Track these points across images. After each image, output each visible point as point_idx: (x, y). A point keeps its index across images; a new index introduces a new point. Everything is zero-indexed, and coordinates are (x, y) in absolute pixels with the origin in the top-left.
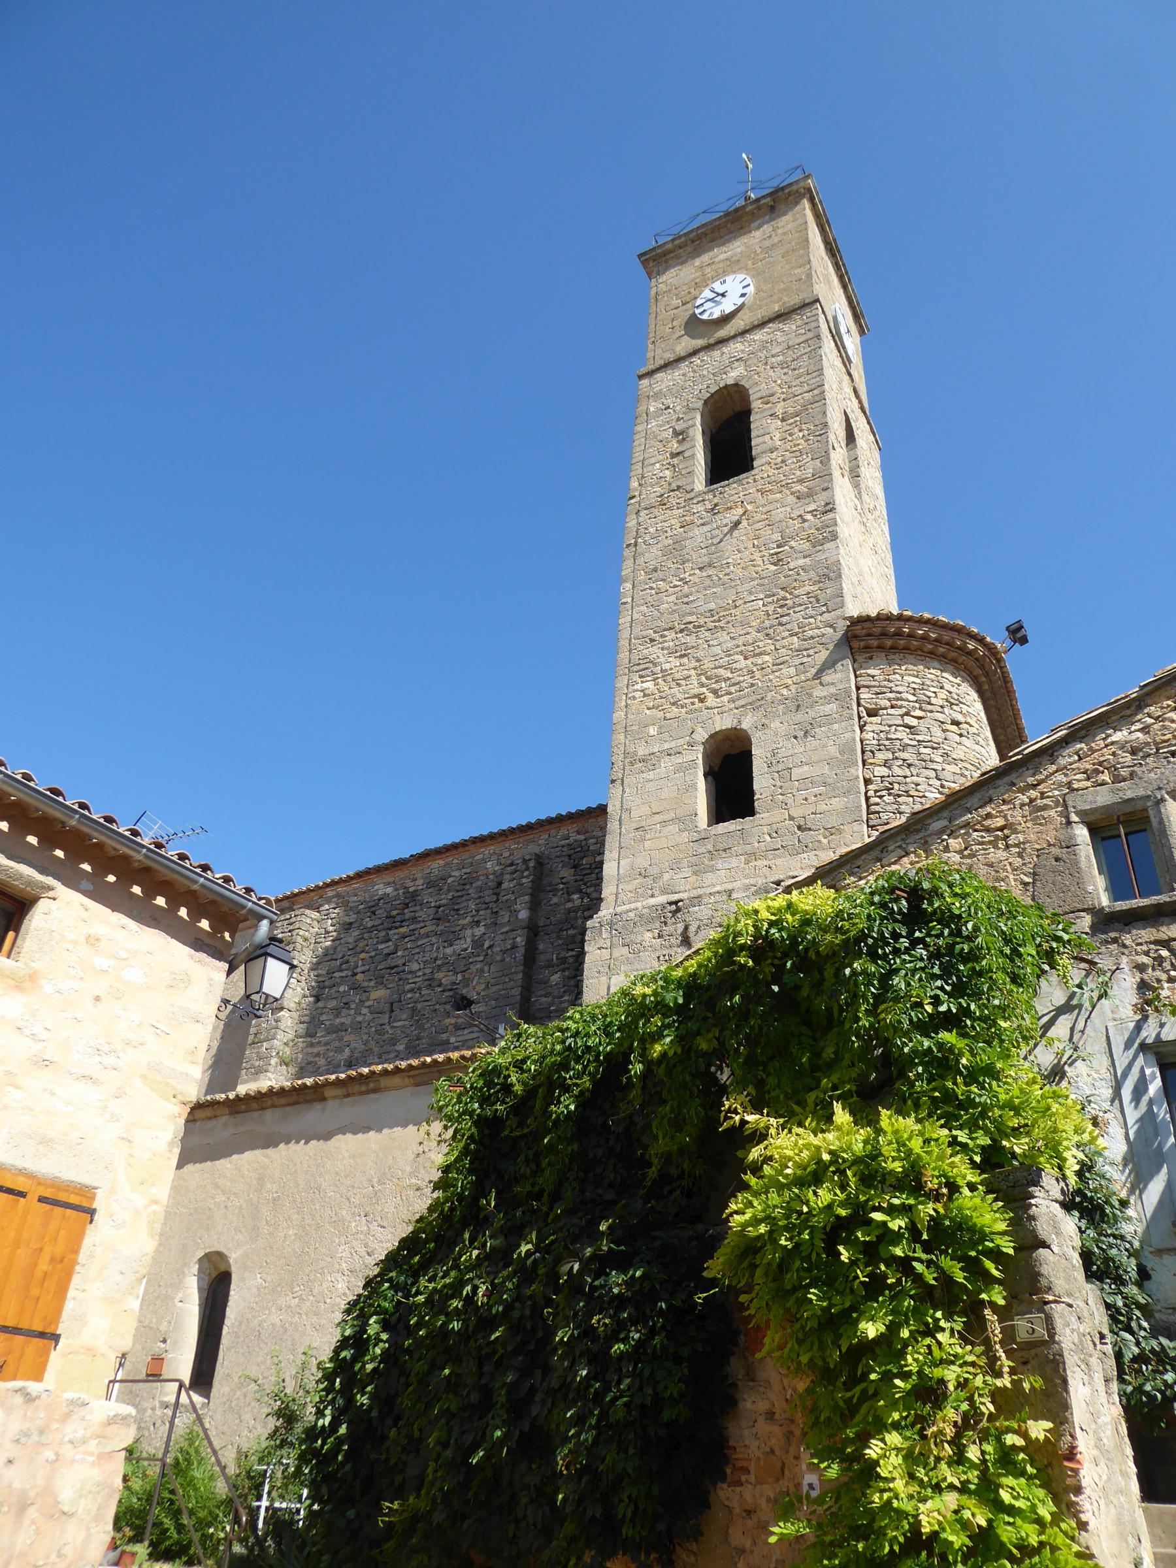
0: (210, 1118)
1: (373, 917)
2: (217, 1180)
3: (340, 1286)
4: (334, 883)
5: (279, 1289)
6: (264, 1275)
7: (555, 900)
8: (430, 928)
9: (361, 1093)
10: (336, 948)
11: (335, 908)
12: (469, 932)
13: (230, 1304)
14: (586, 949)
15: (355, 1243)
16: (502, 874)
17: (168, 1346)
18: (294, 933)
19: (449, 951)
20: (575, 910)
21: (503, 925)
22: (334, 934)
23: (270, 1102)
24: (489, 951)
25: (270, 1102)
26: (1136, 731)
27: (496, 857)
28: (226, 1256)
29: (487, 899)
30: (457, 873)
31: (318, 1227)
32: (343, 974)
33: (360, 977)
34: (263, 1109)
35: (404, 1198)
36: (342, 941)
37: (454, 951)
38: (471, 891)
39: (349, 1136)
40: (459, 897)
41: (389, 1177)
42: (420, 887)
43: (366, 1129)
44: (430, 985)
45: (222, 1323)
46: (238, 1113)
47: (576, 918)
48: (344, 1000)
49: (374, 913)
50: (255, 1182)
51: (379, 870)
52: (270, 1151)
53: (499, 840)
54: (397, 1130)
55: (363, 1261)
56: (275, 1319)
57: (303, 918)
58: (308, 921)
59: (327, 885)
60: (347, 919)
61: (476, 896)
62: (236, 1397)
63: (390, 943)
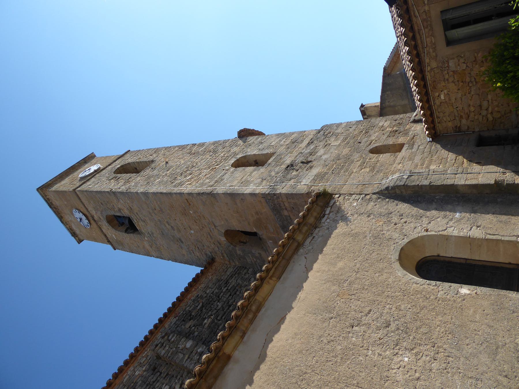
9: (252, 321)
35: (355, 292)
43: (283, 319)
55: (392, 332)
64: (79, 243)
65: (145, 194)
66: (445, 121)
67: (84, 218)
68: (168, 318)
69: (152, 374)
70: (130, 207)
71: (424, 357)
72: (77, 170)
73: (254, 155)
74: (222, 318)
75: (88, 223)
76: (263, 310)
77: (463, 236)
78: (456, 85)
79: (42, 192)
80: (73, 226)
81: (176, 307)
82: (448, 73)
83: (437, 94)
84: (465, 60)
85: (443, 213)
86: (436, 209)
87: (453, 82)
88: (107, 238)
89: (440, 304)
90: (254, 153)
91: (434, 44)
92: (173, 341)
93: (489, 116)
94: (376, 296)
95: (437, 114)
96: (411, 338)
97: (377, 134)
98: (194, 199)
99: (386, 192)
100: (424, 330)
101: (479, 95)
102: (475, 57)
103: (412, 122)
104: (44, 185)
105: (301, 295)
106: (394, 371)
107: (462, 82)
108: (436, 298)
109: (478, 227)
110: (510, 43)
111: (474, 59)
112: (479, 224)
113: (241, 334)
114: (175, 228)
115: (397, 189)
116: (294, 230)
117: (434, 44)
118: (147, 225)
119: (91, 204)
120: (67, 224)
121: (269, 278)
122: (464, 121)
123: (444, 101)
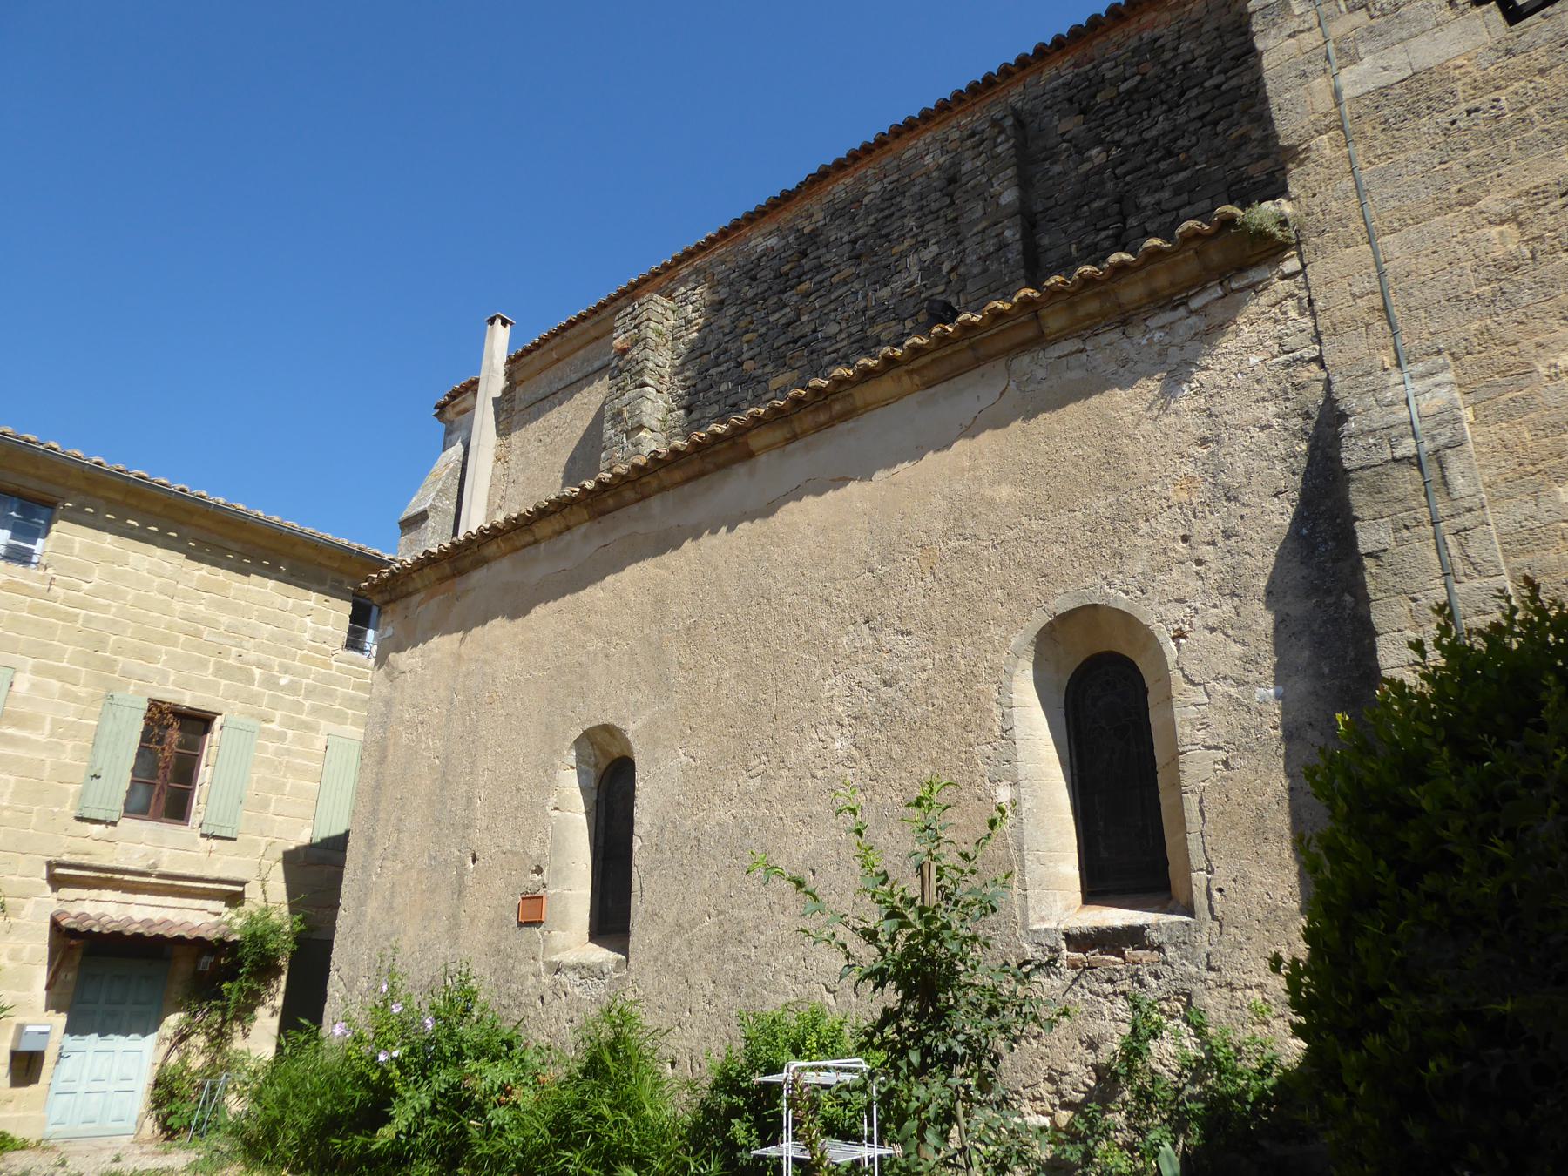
0: (560, 533)
1: (754, 284)
2: (586, 619)
3: (838, 745)
4: (689, 255)
5: (722, 767)
6: (690, 749)
7: (1057, 168)
8: (846, 272)
9: (819, 428)
10: (705, 338)
11: (694, 289)
12: (912, 259)
13: (637, 802)
14: (1260, 45)
15: (853, 671)
16: (952, 165)
17: (546, 877)
18: (642, 327)
19: (884, 293)
20: (1099, 170)
21: (975, 222)
22: (700, 321)
23: (655, 484)
24: (953, 276)
25: (655, 484)
27: (938, 145)
28: (619, 730)
29: (934, 206)
30: (876, 187)
31: (776, 657)
32: (722, 369)
33: (748, 365)
35: (942, 576)
36: (713, 327)
37: (894, 293)
38: (905, 203)
39: (809, 501)
40: (886, 217)
41: (903, 548)
42: (821, 223)
43: (841, 481)
44: (862, 348)
45: (631, 833)
46: (603, 513)
47: (1102, 183)
48: (730, 401)
49: (754, 279)
50: (649, 609)
51: (752, 218)
52: (670, 558)
53: (938, 120)
54: (904, 469)
56: (723, 814)
57: (652, 304)
58: (660, 309)
59: (678, 261)
60: (716, 297)
61: (916, 207)
62: (674, 947)
63: (788, 310)
71: (850, 771)
74: (1125, 175)
77: (1179, 736)
86: (1281, 625)
89: (959, 759)
94: (944, 624)
96: (877, 735)
100: (897, 751)
106: (815, 736)
108: (971, 745)
109: (1226, 763)
113: (788, 436)
116: (1055, 292)
121: (907, 371)
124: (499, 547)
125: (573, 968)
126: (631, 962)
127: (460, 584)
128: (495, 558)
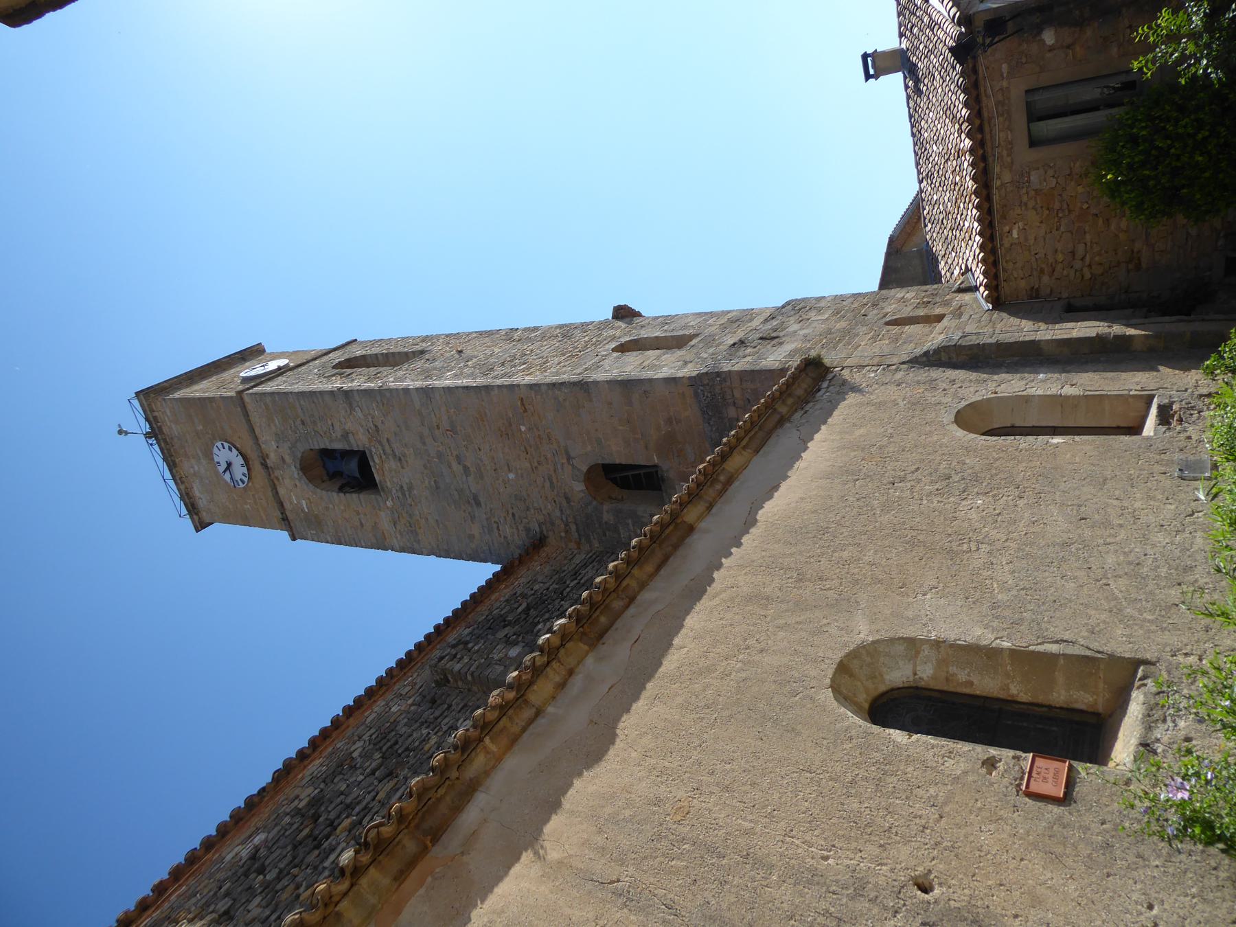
9: (721, 493)
23: (634, 584)
26: (403, 752)
34: (632, 600)
46: (601, 635)
62: (1136, 614)
64: (197, 531)
65: (427, 392)
66: (1015, 278)
67: (238, 461)
68: (453, 628)
69: (431, 708)
70: (376, 426)
72: (225, 370)
73: (656, 337)
75: (244, 474)
76: (736, 484)
78: (1037, 214)
79: (146, 400)
80: (195, 488)
81: (468, 610)
82: (1027, 193)
83: (1007, 228)
84: (1055, 171)
85: (1018, 375)
87: (1034, 208)
88: (284, 510)
90: (656, 335)
91: (1011, 143)
92: (478, 651)
93: (1086, 270)
95: (1004, 264)
97: (894, 306)
98: (539, 397)
99: (924, 359)
101: (1072, 234)
102: (1071, 169)
103: (955, 292)
104: (152, 387)
105: (800, 464)
107: (1048, 209)
109: (1072, 385)
110: (1127, 120)
111: (1068, 172)
112: (1074, 382)
113: (707, 505)
114: (473, 469)
115: (943, 353)
117: (1011, 143)
118: (403, 468)
119: (272, 425)
120: (183, 482)
122: (1046, 279)
123: (1017, 241)
124: (487, 751)
125: (1149, 728)
126: (1148, 656)
127: (452, 841)
128: (487, 773)
